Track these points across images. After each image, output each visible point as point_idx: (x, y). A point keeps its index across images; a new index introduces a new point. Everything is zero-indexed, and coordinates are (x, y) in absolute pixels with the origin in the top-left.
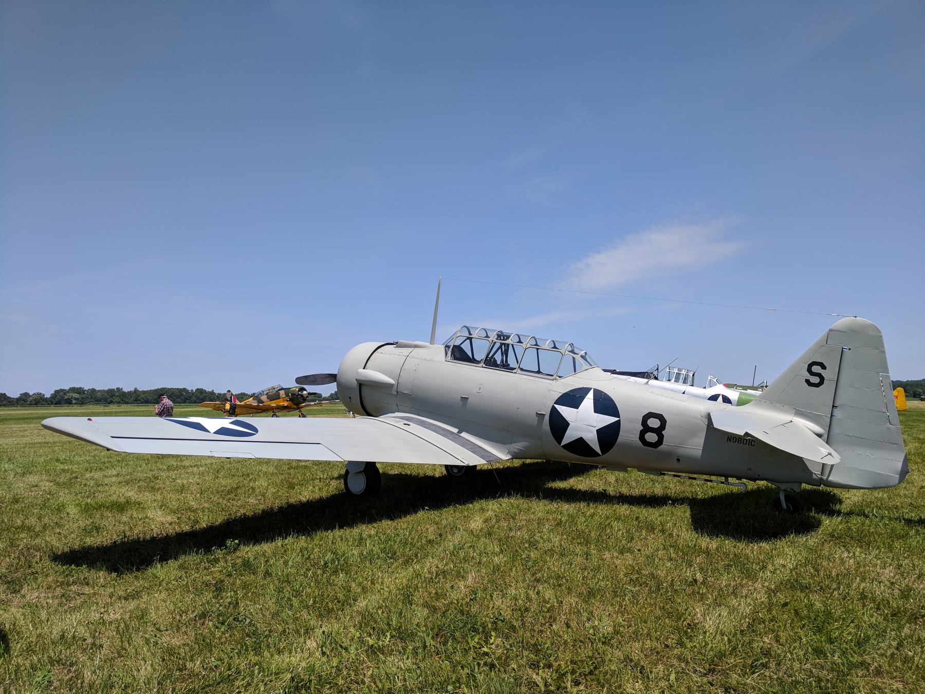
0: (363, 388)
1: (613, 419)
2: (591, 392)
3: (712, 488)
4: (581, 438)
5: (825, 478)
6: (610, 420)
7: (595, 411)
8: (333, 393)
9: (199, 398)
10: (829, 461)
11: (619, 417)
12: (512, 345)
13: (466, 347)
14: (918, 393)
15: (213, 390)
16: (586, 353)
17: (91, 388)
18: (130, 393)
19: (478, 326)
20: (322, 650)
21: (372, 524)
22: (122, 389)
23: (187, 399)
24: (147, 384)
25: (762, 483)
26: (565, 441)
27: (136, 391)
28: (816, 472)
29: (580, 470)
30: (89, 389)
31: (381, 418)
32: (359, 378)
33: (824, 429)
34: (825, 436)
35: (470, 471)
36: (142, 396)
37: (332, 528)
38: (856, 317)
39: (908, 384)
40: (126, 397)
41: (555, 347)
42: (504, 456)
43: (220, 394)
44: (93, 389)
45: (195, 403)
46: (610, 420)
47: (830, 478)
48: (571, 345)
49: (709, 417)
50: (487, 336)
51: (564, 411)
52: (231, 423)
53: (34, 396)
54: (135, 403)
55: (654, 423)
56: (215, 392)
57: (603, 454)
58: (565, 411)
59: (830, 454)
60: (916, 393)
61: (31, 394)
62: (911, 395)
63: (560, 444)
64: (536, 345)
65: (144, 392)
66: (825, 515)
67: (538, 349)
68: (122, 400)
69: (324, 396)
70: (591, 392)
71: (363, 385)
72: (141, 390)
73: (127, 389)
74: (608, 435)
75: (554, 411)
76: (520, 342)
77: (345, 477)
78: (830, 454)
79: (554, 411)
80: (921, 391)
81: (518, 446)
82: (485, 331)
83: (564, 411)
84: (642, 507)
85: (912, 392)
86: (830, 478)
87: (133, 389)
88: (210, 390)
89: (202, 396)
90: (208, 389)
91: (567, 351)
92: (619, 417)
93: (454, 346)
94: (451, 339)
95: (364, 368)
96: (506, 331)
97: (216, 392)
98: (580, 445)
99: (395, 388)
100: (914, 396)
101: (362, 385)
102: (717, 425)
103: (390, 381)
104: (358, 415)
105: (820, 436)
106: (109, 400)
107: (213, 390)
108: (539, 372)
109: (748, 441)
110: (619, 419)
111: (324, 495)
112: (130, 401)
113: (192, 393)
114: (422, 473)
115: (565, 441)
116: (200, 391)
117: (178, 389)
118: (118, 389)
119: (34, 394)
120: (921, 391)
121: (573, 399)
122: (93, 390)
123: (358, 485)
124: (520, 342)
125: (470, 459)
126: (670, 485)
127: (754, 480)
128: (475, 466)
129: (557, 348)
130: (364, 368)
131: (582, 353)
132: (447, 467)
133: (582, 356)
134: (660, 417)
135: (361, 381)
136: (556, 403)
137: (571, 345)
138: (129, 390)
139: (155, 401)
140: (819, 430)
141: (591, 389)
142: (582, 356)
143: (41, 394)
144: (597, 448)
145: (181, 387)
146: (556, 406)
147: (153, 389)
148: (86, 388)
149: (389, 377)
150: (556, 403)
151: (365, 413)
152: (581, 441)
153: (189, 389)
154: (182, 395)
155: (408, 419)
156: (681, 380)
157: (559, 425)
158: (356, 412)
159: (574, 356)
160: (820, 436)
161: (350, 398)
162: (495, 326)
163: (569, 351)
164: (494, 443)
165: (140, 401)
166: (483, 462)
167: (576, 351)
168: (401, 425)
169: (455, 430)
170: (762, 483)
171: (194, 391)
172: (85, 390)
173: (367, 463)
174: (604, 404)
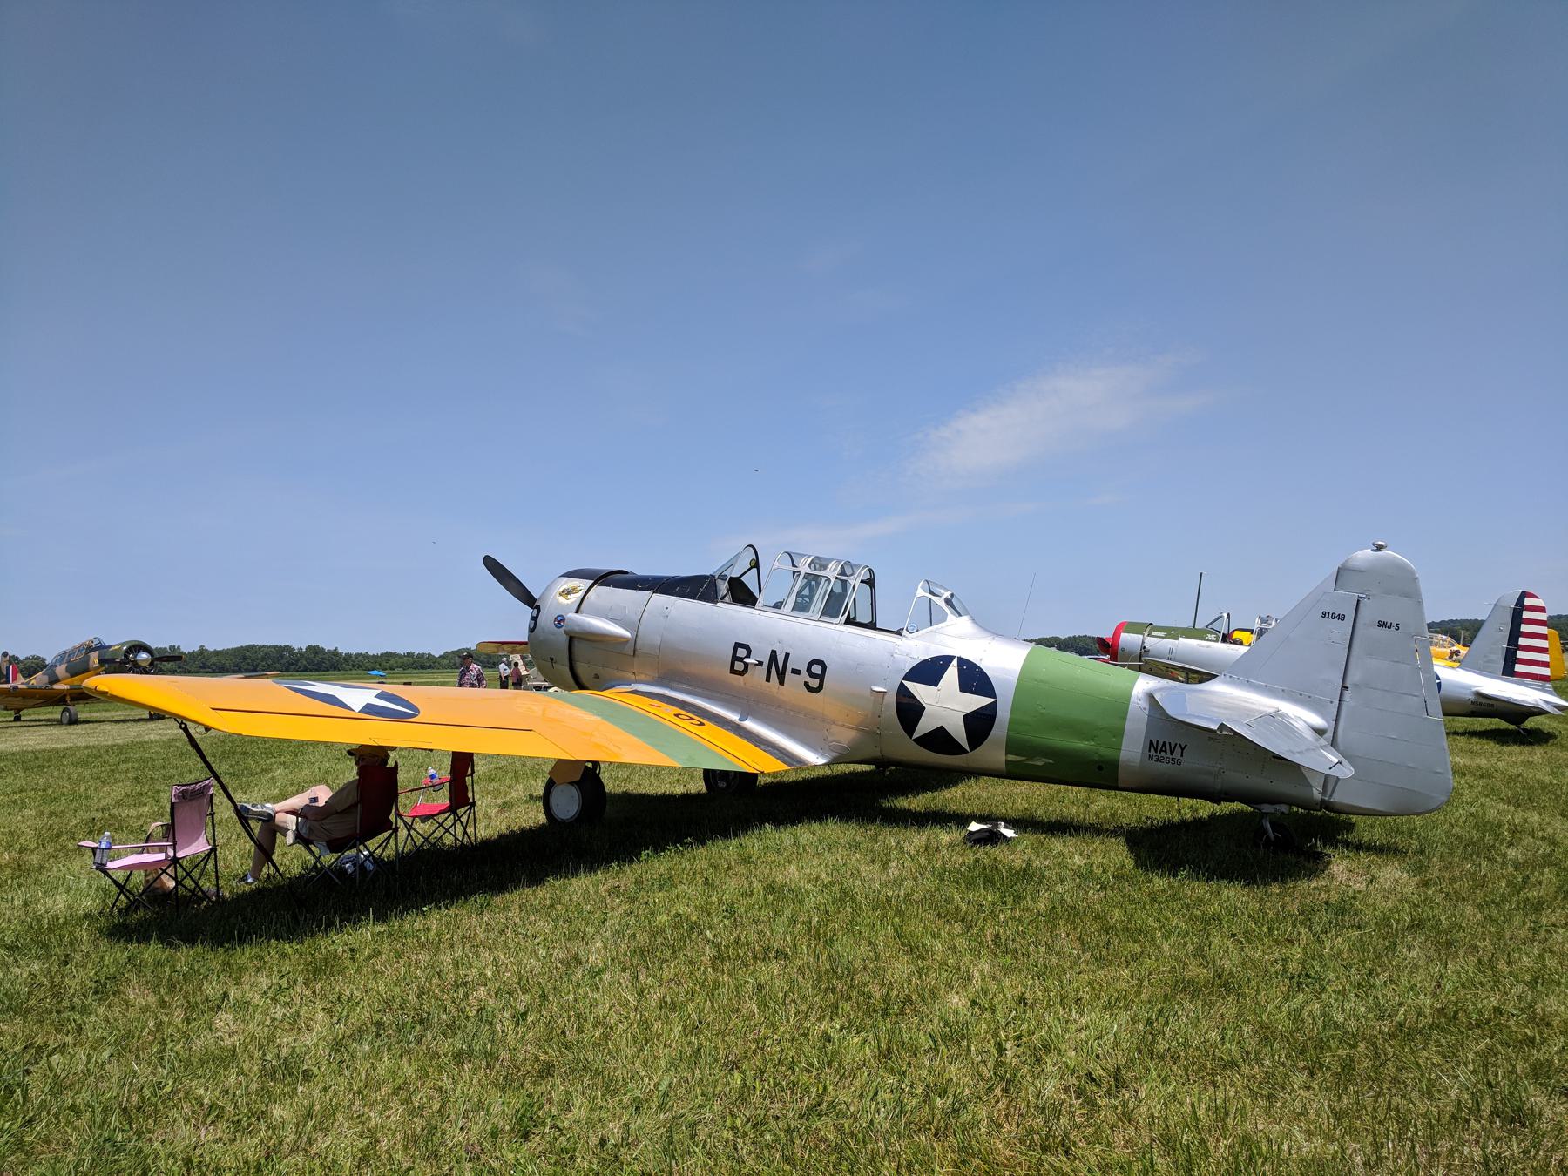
0: (576, 643)
4: (941, 728)
6: (981, 701)
7: (966, 717)
9: (313, 662)
11: (995, 697)
13: (750, 581)
15: (336, 649)
16: (952, 595)
18: (192, 655)
22: (179, 648)
23: (293, 664)
24: (221, 640)
26: (919, 732)
27: (202, 651)
29: (950, 777)
31: (616, 696)
34: (1329, 735)
35: (745, 781)
36: (214, 660)
37: (575, 873)
38: (1380, 548)
42: (814, 758)
43: (349, 655)
45: (305, 670)
46: (981, 701)
51: (918, 689)
53: (26, 662)
56: (340, 650)
58: (919, 690)
61: (21, 659)
65: (216, 653)
68: (179, 668)
74: (979, 723)
75: (903, 691)
78: (1340, 763)
79: (903, 691)
82: (790, 555)
83: (918, 689)
87: (197, 649)
88: (332, 648)
89: (317, 659)
90: (328, 646)
92: (995, 697)
94: (730, 565)
95: (577, 612)
97: (343, 650)
98: (939, 739)
99: (628, 649)
101: (576, 639)
107: (336, 649)
110: (993, 700)
113: (301, 654)
115: (919, 732)
116: (315, 650)
117: (275, 647)
119: (27, 658)
121: (929, 671)
123: (568, 804)
125: (764, 765)
126: (1102, 804)
130: (577, 612)
131: (947, 595)
132: (709, 775)
134: (822, 663)
135: (571, 632)
136: (906, 678)
139: (237, 668)
140: (1318, 721)
143: (38, 658)
144: (965, 744)
145: (282, 643)
146: (908, 684)
147: (234, 647)
149: (624, 628)
150: (906, 678)
152: (941, 731)
153: (296, 646)
154: (282, 656)
156: (819, 603)
157: (909, 710)
158: (554, 680)
161: (552, 659)
166: (783, 767)
174: (974, 678)
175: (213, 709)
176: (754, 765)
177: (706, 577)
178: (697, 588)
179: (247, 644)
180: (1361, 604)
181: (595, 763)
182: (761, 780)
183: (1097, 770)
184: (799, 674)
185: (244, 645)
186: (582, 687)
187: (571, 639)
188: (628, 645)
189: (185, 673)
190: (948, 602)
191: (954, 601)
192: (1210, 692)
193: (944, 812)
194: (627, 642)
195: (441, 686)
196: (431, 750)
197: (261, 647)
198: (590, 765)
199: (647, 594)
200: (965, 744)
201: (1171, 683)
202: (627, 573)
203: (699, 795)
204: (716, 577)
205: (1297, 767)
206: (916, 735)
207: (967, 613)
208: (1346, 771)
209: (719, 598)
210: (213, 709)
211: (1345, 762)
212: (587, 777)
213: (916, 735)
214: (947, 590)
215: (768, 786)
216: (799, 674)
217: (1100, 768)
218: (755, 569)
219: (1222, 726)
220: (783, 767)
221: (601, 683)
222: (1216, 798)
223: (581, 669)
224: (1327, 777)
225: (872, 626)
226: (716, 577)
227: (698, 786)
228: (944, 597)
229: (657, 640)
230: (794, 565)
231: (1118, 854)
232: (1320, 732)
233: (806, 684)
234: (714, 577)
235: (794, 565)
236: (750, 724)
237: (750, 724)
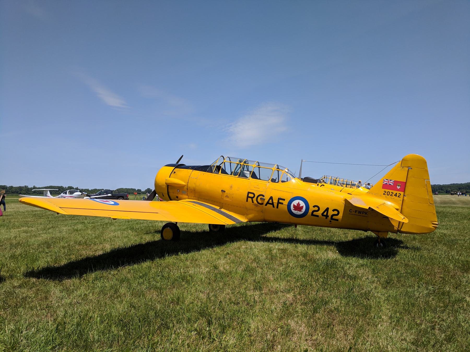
0: (169, 187)
3: (351, 235)
5: (399, 229)
8: (147, 189)
10: (404, 221)
14: (449, 190)
15: (77, 187)
20: (57, 327)
21: (177, 254)
22: (28, 186)
25: (369, 233)
28: (396, 225)
31: (179, 201)
32: (167, 182)
33: (399, 207)
34: (400, 209)
35: (222, 227)
39: (443, 186)
40: (29, 191)
47: (401, 230)
54: (34, 194)
55: (251, 195)
59: (404, 218)
60: (448, 191)
62: (445, 192)
68: (27, 193)
69: (142, 191)
71: (170, 185)
73: (30, 186)
77: (161, 232)
80: (450, 189)
81: (251, 216)
85: (445, 191)
86: (401, 230)
93: (217, 166)
94: (215, 162)
99: (185, 187)
100: (447, 192)
101: (168, 186)
103: (183, 183)
104: (393, 223)
105: (397, 210)
106: (19, 192)
107: (77, 187)
111: (242, 242)
112: (31, 193)
114: (194, 230)
118: (25, 186)
120: (450, 189)
122: (12, 187)
123: (169, 234)
125: (227, 222)
127: (366, 231)
128: (224, 225)
135: (168, 183)
140: (398, 207)
148: (8, 186)
155: (194, 202)
160: (397, 210)
164: (241, 216)
165: (36, 193)
166: (233, 223)
168: (192, 206)
169: (218, 208)
170: (369, 233)
171: (67, 188)
172: (8, 187)
176: (225, 222)
177: (209, 166)
180: (409, 170)
181: (177, 223)
184: (285, 200)
185: (48, 186)
186: (171, 200)
187: (168, 185)
188: (185, 187)
189: (29, 194)
194: (185, 186)
195: (212, 210)
198: (175, 223)
202: (185, 165)
203: (3, 204)
204: (212, 166)
205: (387, 218)
207: (296, 177)
208: (406, 221)
209: (213, 172)
211: (405, 218)
212: (172, 226)
216: (285, 200)
219: (370, 208)
220: (233, 223)
221: (177, 199)
223: (171, 194)
224: (400, 222)
225: (260, 179)
226: (212, 166)
227: (207, 229)
229: (194, 186)
230: (230, 161)
233: (352, 210)
234: (211, 166)
235: (230, 161)
236: (222, 210)
237: (222, 210)
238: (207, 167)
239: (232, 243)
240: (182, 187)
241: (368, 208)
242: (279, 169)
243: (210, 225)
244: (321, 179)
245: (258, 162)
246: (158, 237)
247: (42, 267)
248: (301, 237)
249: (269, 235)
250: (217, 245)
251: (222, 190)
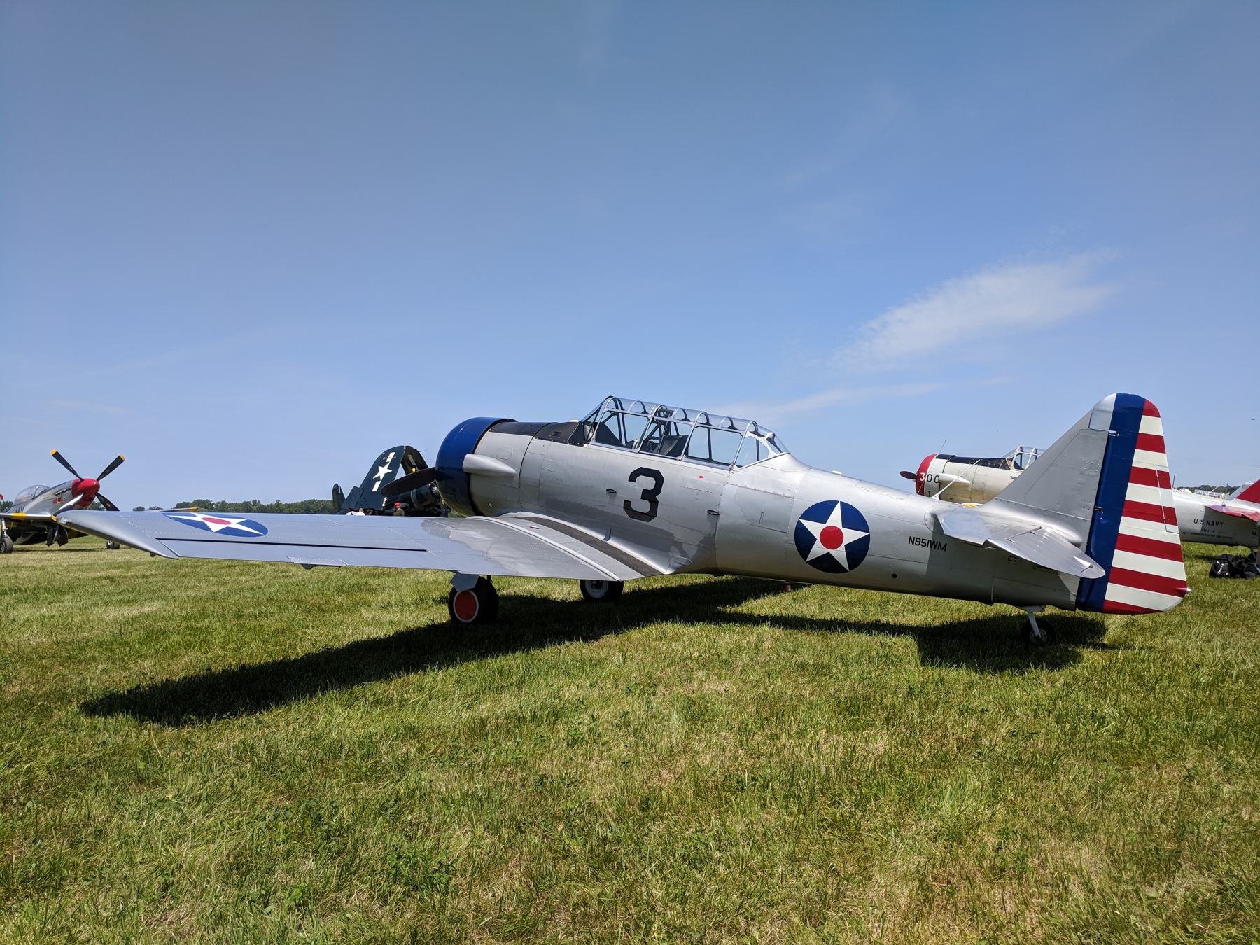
1: (864, 534)
2: (839, 505)
12: (675, 423)
13: (612, 425)
16: (774, 435)
17: (221, 501)
19: (631, 394)
22: (259, 502)
30: (218, 503)
41: (732, 427)
44: (224, 502)
48: (755, 424)
49: (935, 517)
50: (645, 412)
52: (239, 523)
57: (850, 570)
63: (805, 559)
64: (708, 423)
66: (1042, 668)
67: (709, 429)
70: (839, 505)
72: (283, 503)
74: (858, 551)
76: (686, 419)
82: (685, 412)
84: (898, 624)
91: (748, 432)
96: (669, 404)
99: (516, 478)
102: (949, 530)
103: (969, 482)
108: (710, 460)
109: (988, 550)
118: (254, 501)
121: (820, 511)
124: (686, 419)
125: (611, 571)
129: (736, 429)
131: (769, 435)
133: (769, 439)
136: (802, 518)
137: (755, 424)
138: (269, 504)
141: (837, 502)
142: (769, 439)
144: (846, 566)
146: (804, 522)
150: (802, 518)
151: (472, 512)
159: (759, 438)
162: (656, 400)
163: (751, 432)
167: (760, 431)
169: (601, 537)
172: (213, 504)
173: (480, 579)
175: (157, 539)
177: (1002, 459)
178: (576, 435)
179: (309, 499)
181: (489, 577)
182: (627, 588)
183: (892, 579)
190: (771, 440)
191: (775, 440)
192: (981, 514)
193: (742, 614)
196: (340, 567)
197: (320, 502)
198: (486, 578)
199: (529, 438)
200: (846, 566)
201: (950, 504)
205: (1056, 573)
206: (809, 559)
210: (157, 539)
213: (809, 559)
214: (769, 431)
215: (633, 594)
217: (894, 576)
218: (616, 417)
222: (987, 600)
227: (575, 593)
228: (767, 437)
231: (905, 646)
232: (1077, 545)
236: (611, 542)
237: (611, 542)
238: (1000, 460)
239: (319, 693)
240: (966, 486)
241: (982, 543)
242: (710, 425)
243: (583, 583)
244: (1010, 457)
245: (705, 414)
246: (442, 615)
247: (162, 680)
248: (765, 629)
249: (746, 607)
250: (746, 600)
251: (608, 490)
